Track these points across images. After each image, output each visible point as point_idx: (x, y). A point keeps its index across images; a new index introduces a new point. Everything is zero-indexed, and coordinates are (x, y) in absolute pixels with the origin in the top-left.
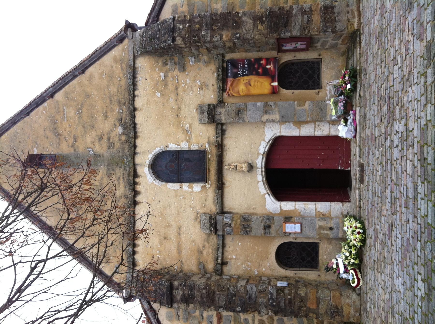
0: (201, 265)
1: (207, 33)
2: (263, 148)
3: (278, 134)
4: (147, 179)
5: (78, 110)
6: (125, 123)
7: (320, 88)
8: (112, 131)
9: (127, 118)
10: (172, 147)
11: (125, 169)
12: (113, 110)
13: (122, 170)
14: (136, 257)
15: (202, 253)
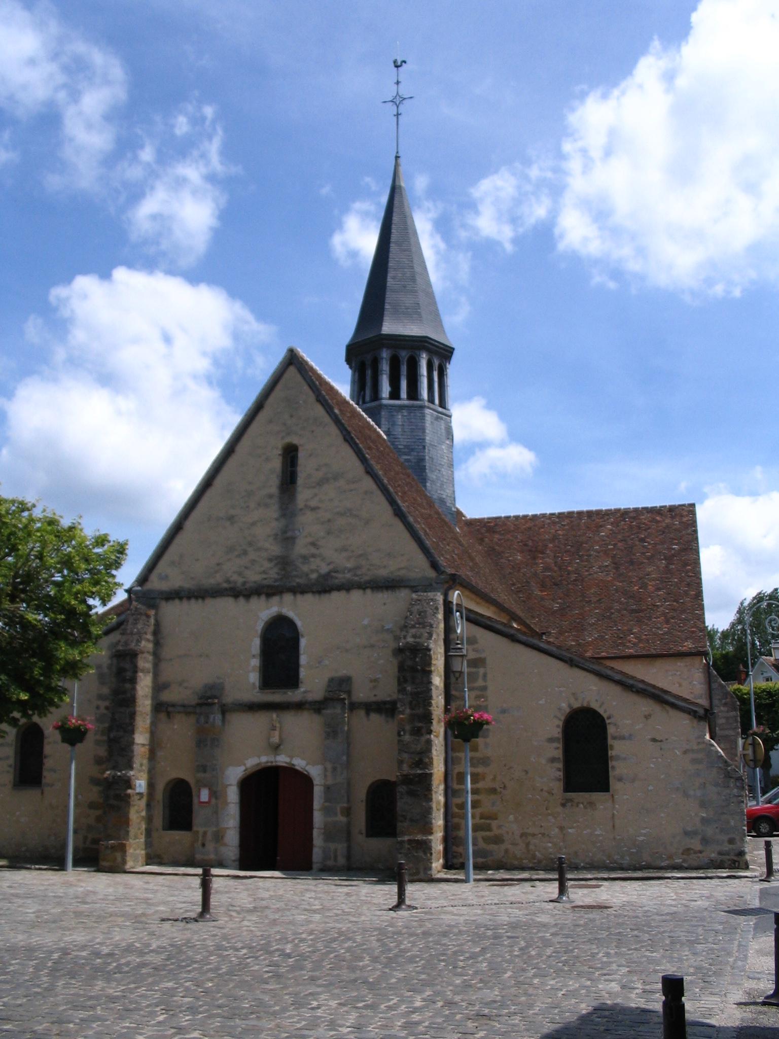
2: (299, 763)
3: (315, 782)
4: (265, 611)
6: (332, 577)
8: (323, 559)
10: (303, 642)
11: (276, 580)
12: (348, 559)
13: (276, 576)
15: (180, 685)
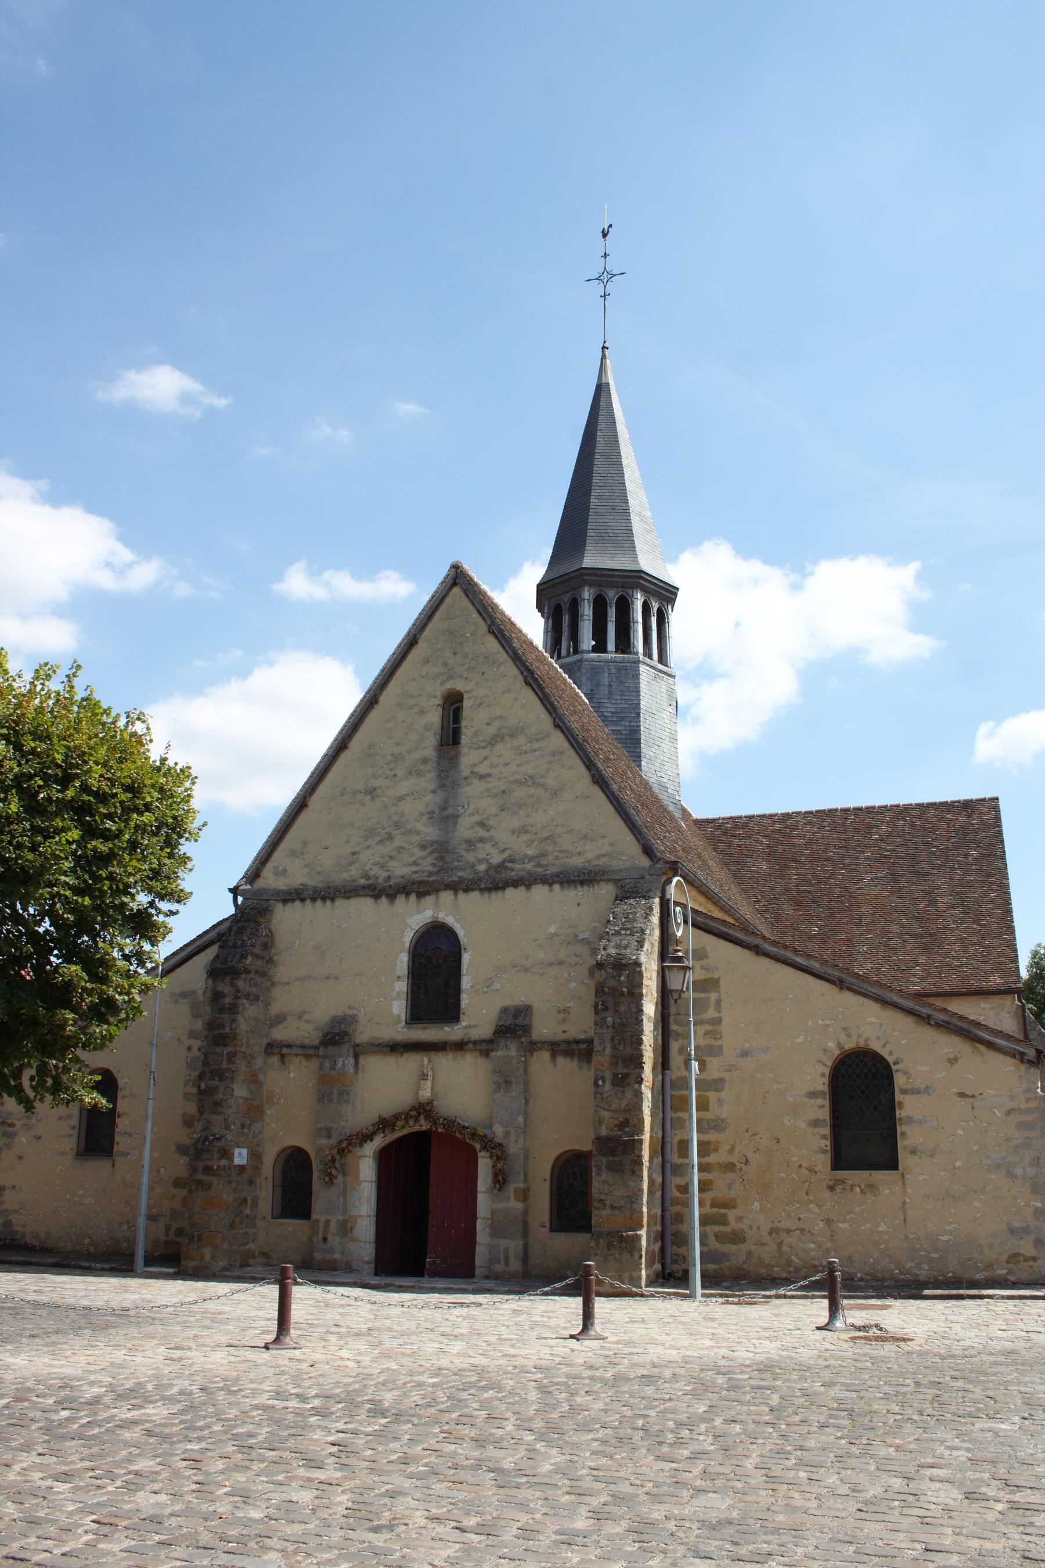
0: (280, 1019)
1: (608, 1027)
4: (415, 916)
6: (507, 868)
7: (552, 1230)
9: (514, 873)
10: (466, 958)
11: (431, 874)
13: (430, 868)
14: (298, 903)
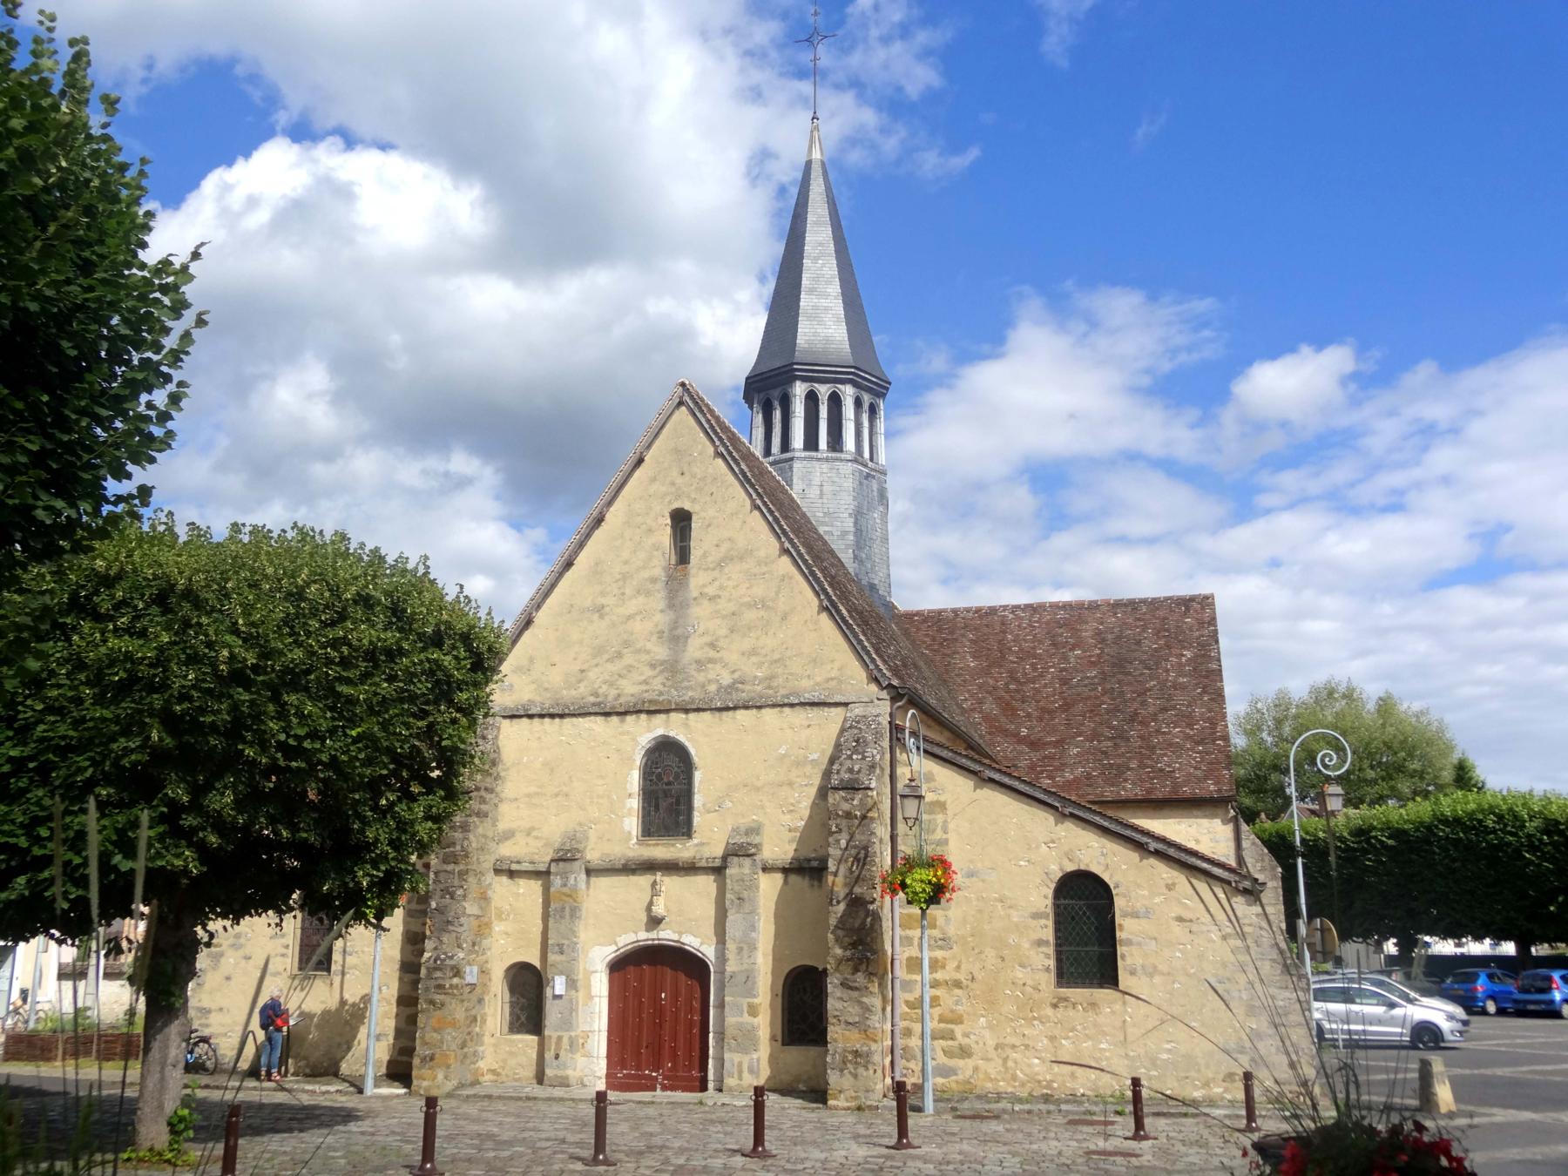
4: (646, 732)
5: (763, 601)
